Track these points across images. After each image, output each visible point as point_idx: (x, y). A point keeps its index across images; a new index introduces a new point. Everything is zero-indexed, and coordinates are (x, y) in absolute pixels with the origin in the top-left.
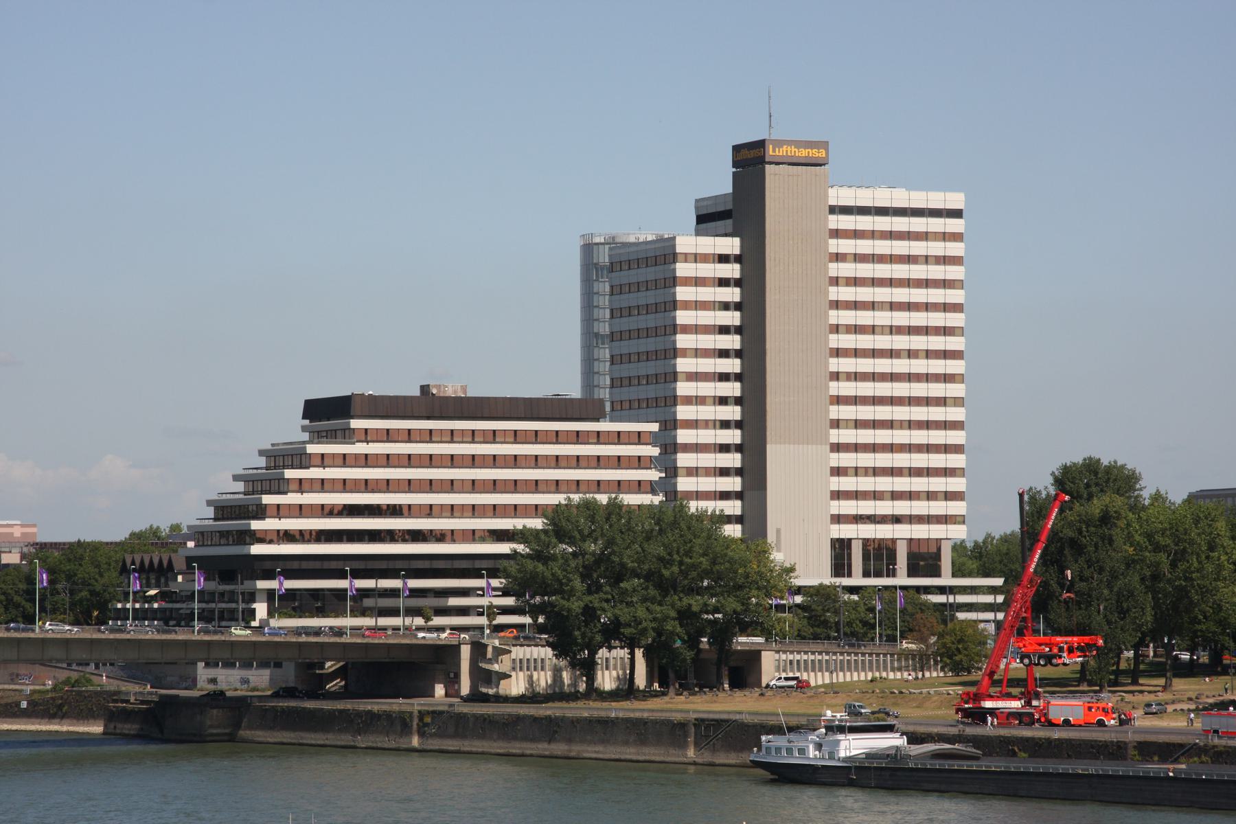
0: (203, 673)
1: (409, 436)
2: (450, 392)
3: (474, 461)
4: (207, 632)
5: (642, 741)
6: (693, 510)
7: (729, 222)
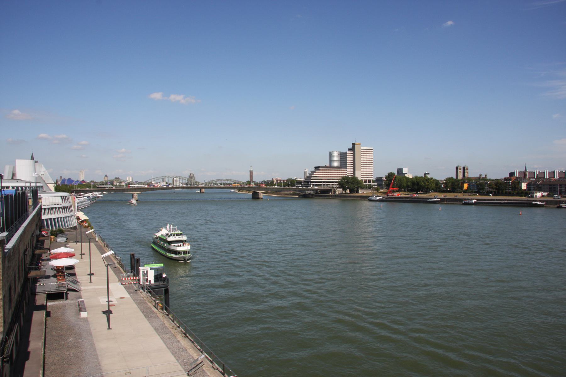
0: (306, 192)
1: (325, 170)
3: (330, 172)
5: (354, 198)
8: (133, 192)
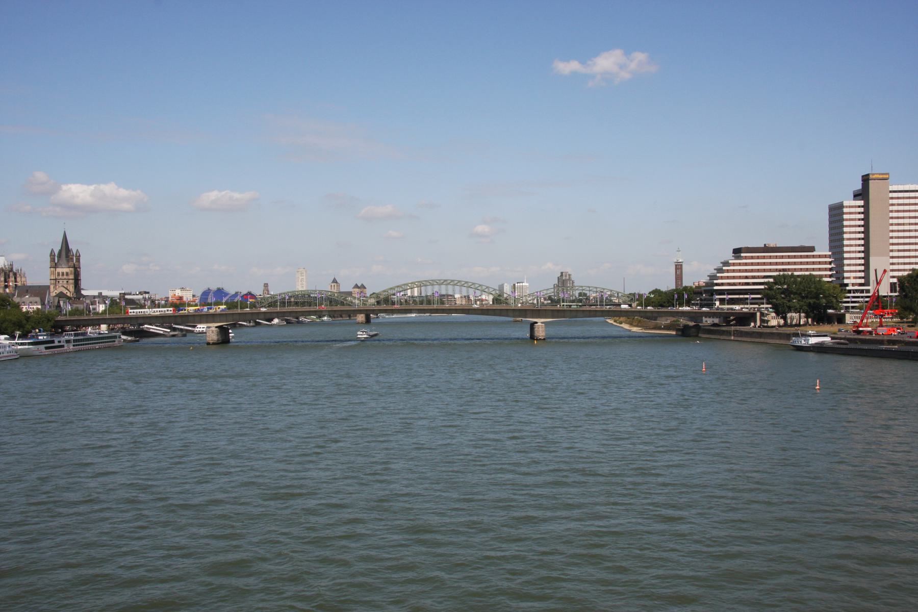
5: (780, 339)
6: (24, 310)
8: (533, 318)
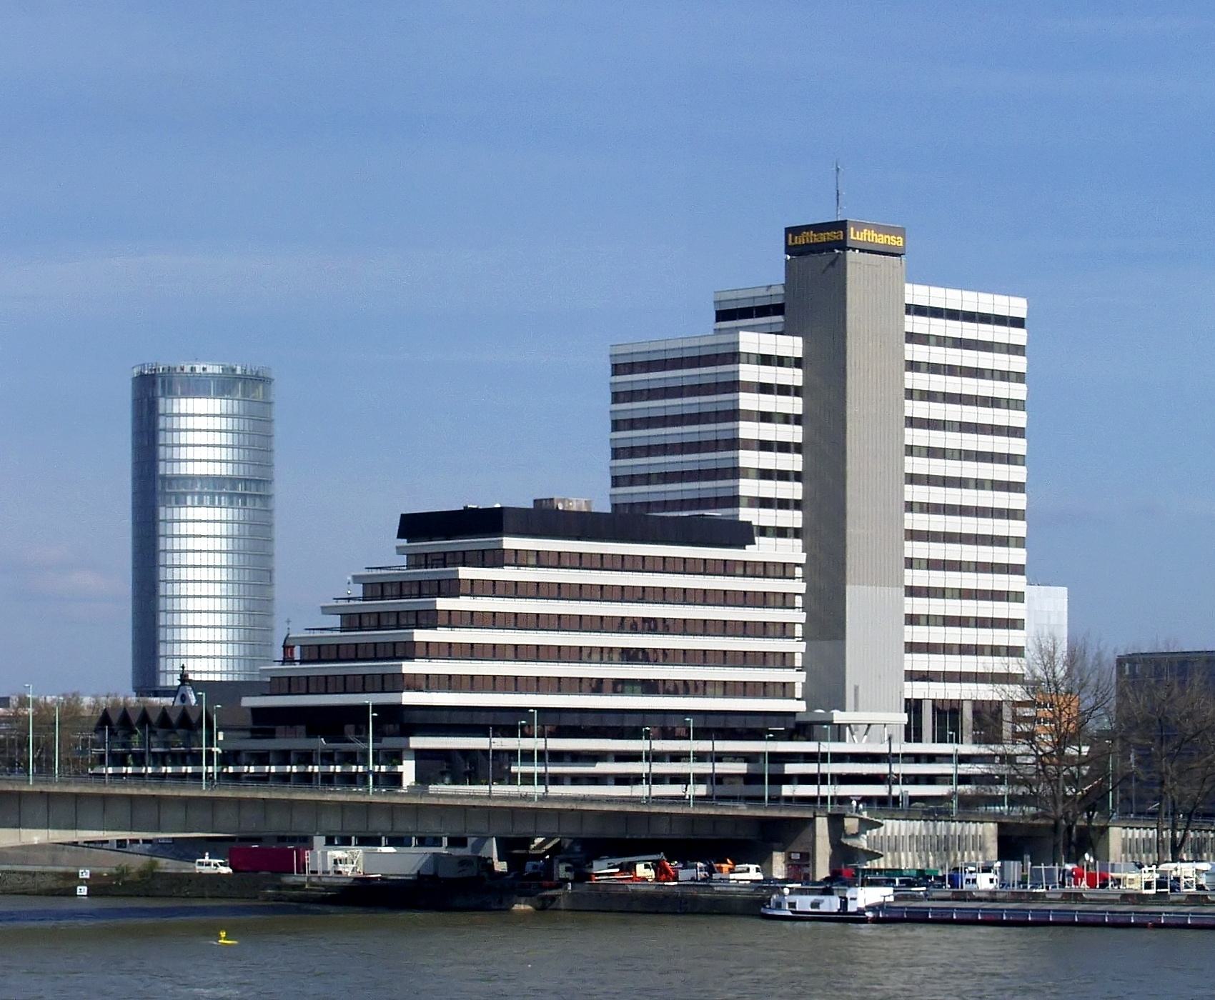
2: (574, 506)
4: (380, 793)
7: (779, 318)
